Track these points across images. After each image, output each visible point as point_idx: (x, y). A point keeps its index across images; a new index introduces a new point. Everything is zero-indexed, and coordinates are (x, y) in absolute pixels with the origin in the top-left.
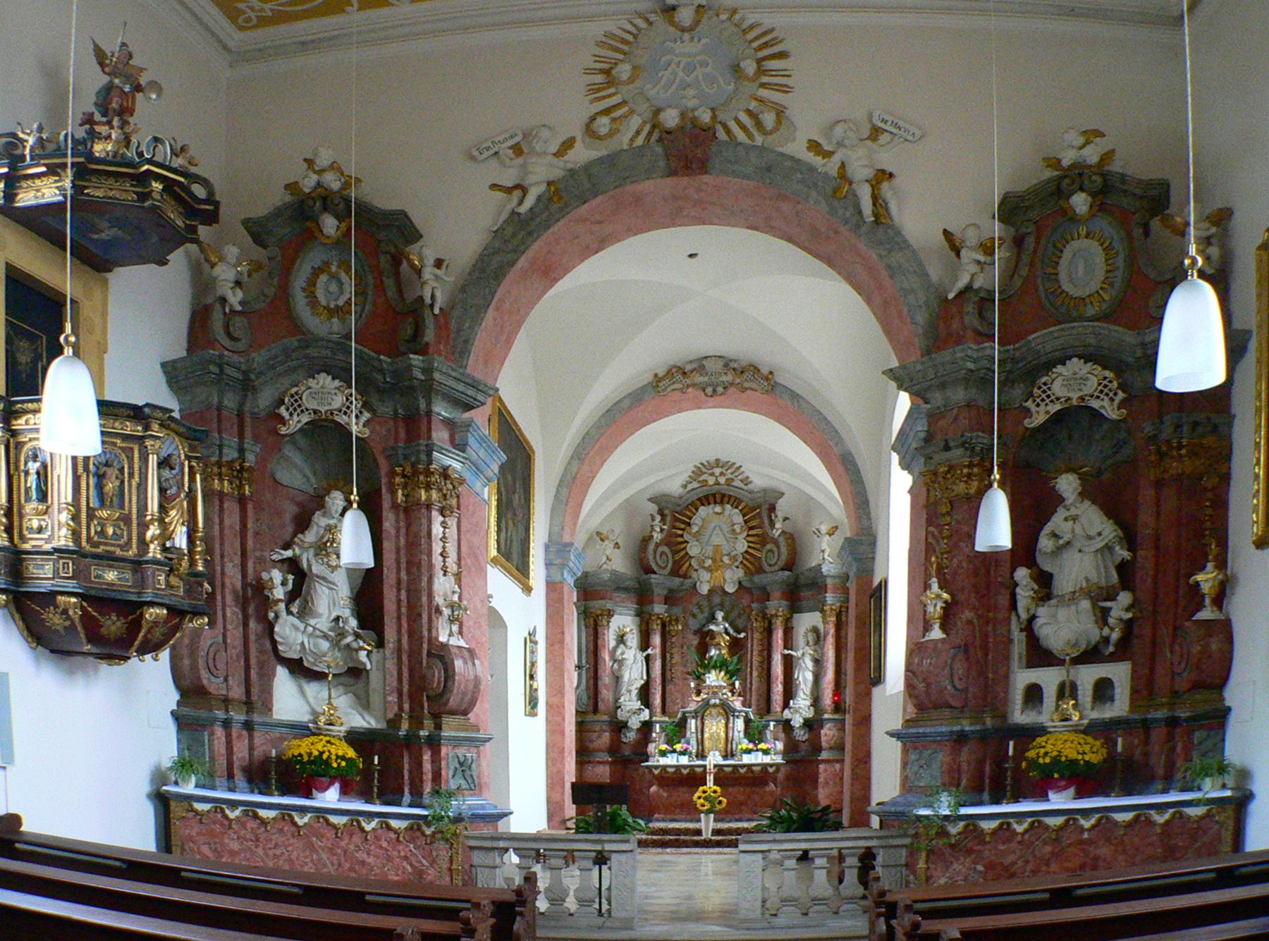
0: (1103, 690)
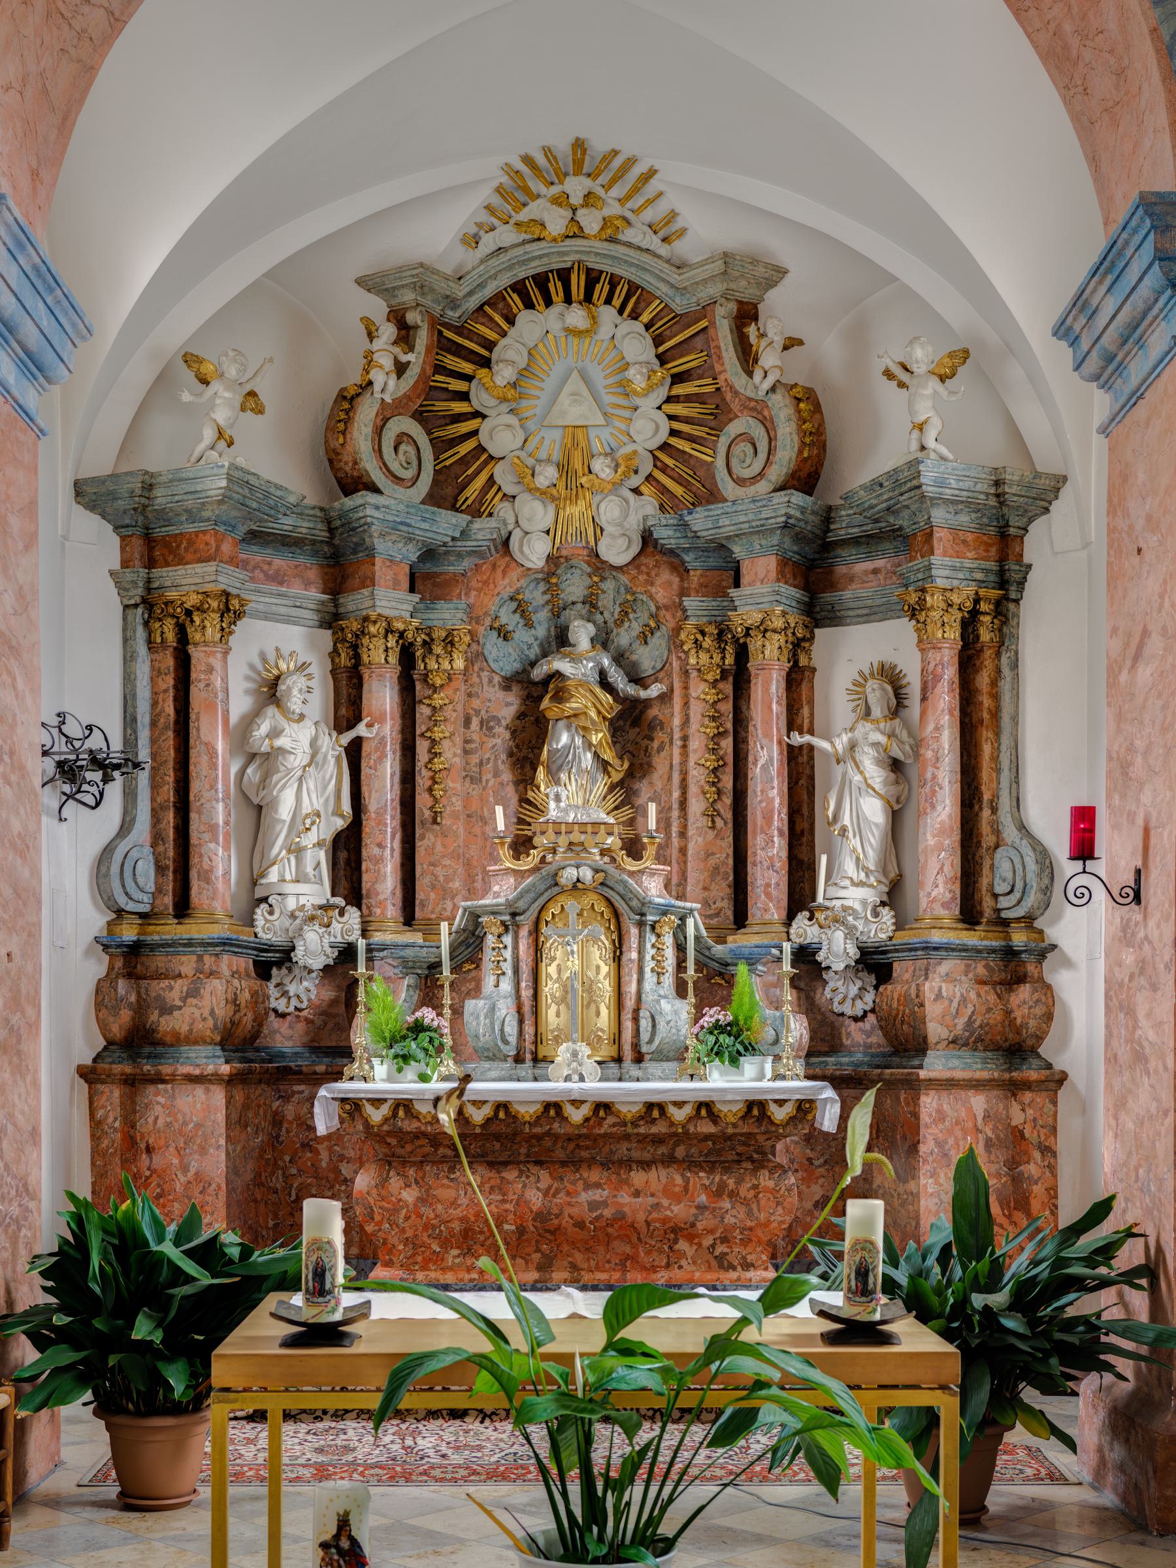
0: (204, 1019)
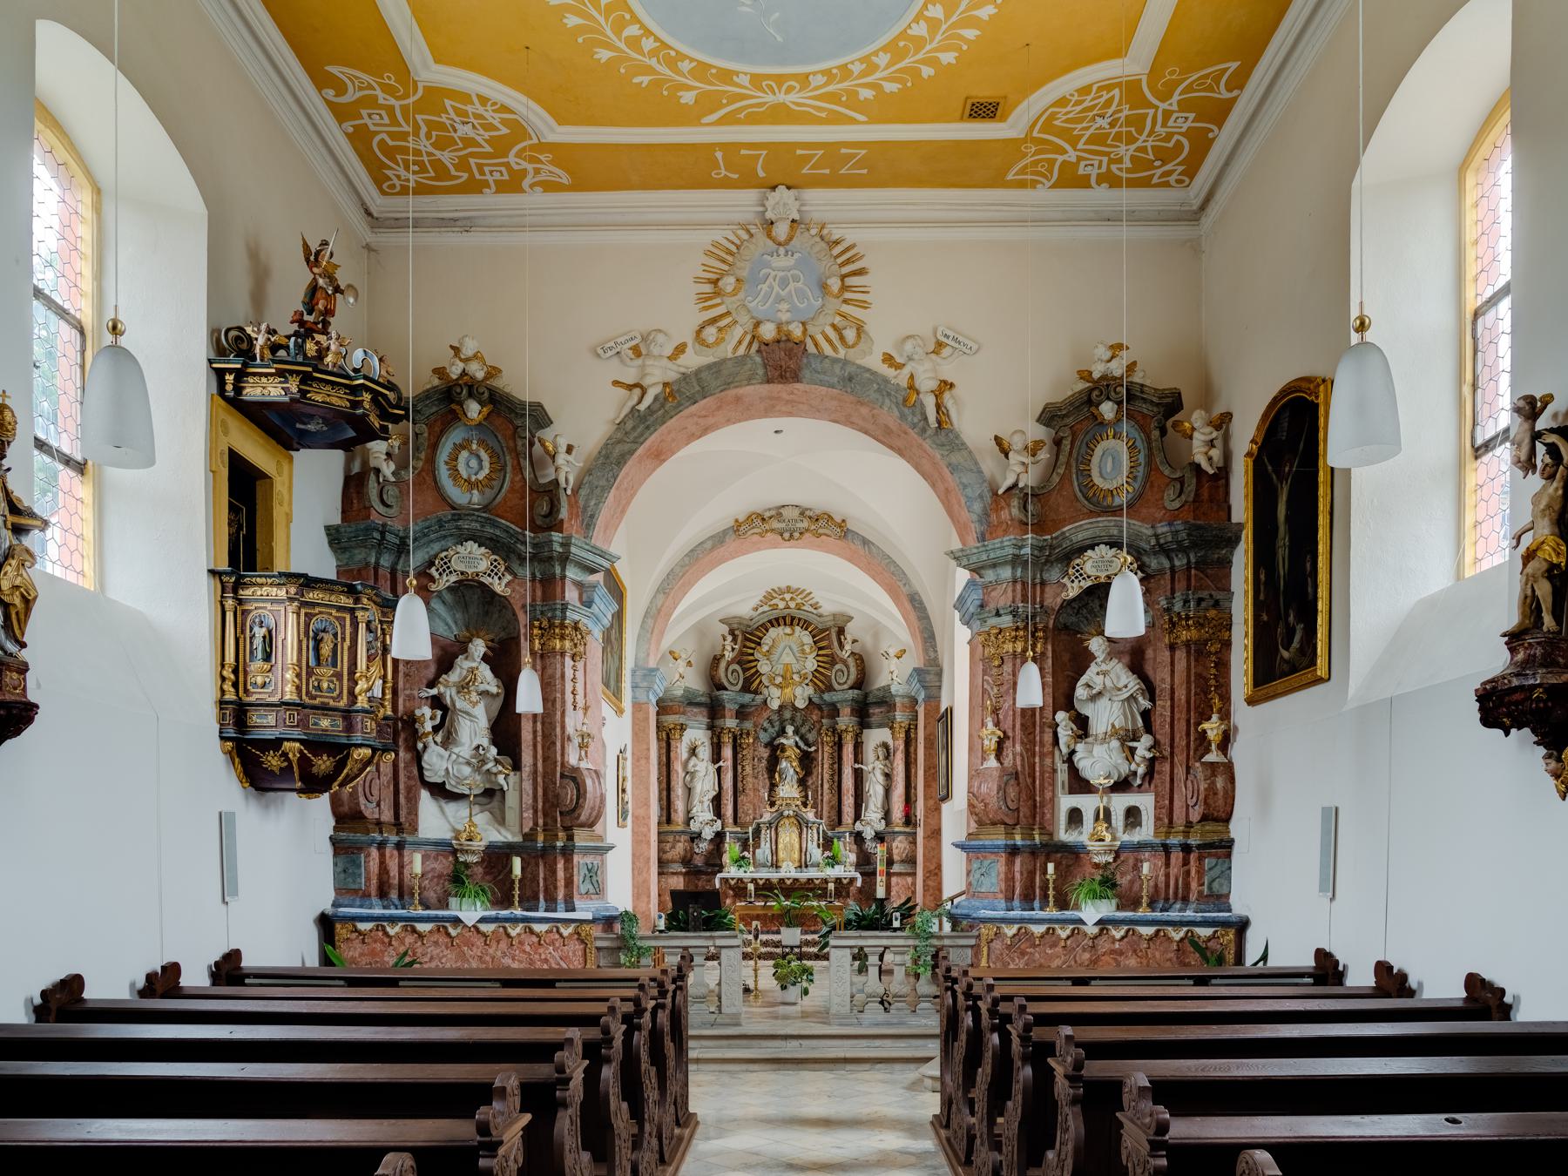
0: (1133, 815)
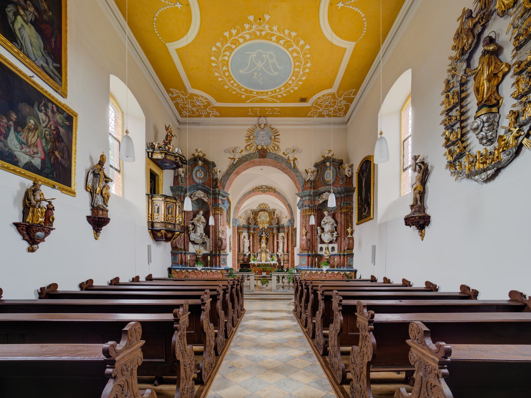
0: (333, 249)
